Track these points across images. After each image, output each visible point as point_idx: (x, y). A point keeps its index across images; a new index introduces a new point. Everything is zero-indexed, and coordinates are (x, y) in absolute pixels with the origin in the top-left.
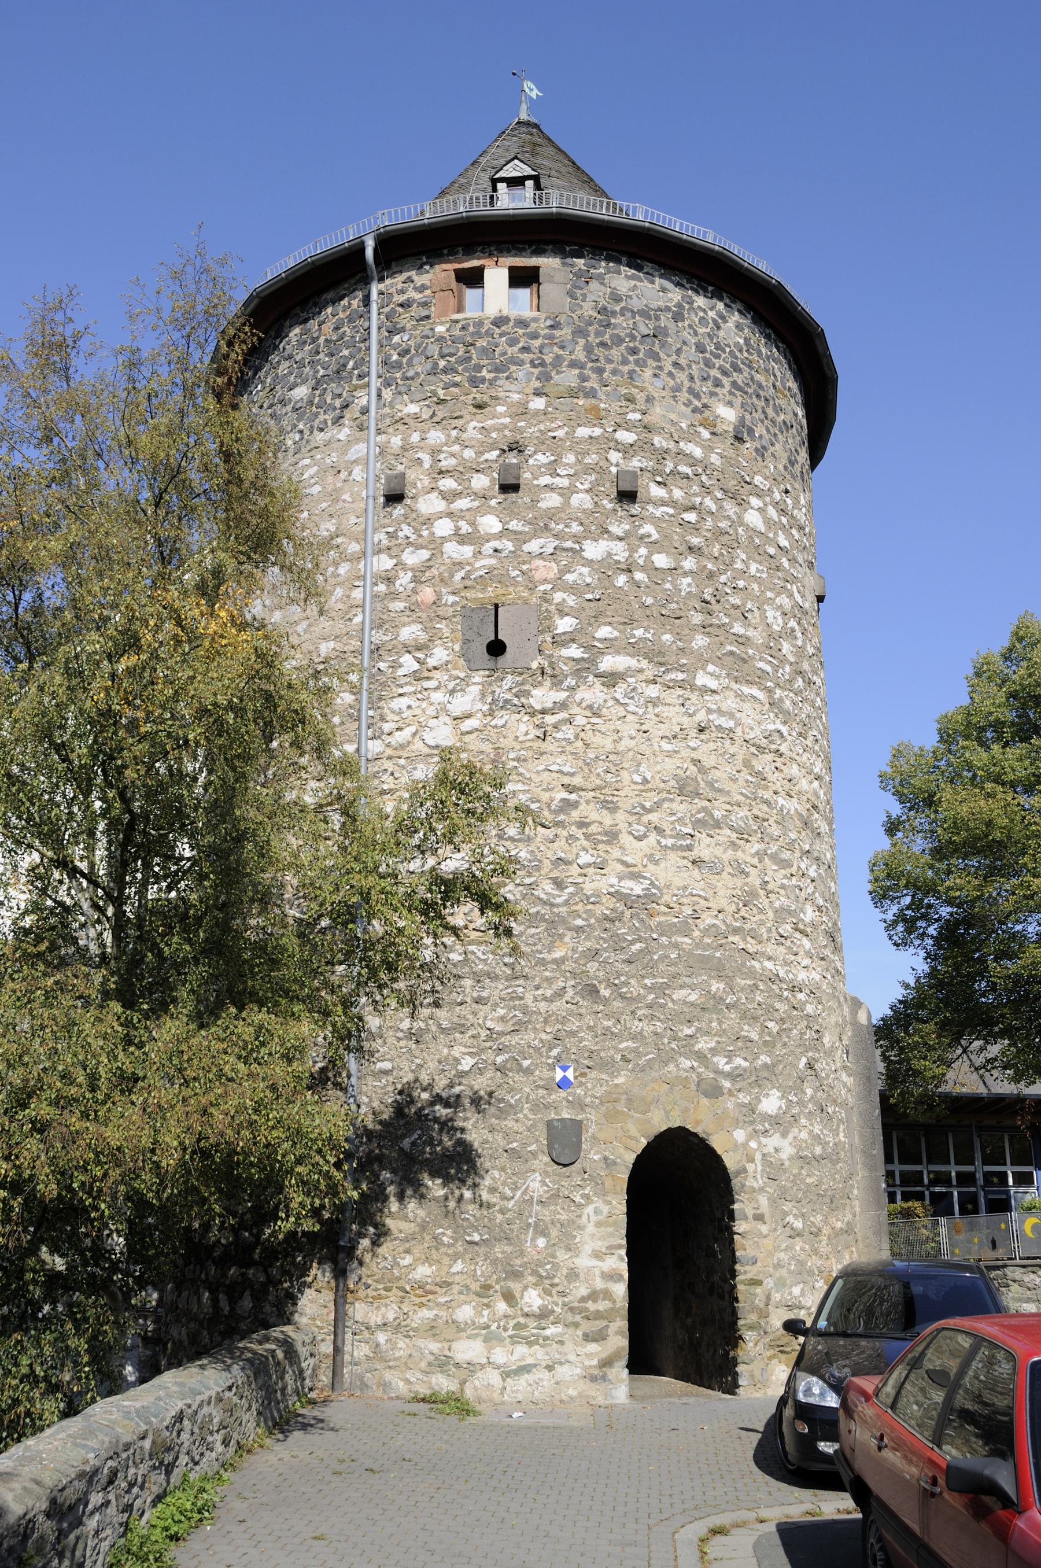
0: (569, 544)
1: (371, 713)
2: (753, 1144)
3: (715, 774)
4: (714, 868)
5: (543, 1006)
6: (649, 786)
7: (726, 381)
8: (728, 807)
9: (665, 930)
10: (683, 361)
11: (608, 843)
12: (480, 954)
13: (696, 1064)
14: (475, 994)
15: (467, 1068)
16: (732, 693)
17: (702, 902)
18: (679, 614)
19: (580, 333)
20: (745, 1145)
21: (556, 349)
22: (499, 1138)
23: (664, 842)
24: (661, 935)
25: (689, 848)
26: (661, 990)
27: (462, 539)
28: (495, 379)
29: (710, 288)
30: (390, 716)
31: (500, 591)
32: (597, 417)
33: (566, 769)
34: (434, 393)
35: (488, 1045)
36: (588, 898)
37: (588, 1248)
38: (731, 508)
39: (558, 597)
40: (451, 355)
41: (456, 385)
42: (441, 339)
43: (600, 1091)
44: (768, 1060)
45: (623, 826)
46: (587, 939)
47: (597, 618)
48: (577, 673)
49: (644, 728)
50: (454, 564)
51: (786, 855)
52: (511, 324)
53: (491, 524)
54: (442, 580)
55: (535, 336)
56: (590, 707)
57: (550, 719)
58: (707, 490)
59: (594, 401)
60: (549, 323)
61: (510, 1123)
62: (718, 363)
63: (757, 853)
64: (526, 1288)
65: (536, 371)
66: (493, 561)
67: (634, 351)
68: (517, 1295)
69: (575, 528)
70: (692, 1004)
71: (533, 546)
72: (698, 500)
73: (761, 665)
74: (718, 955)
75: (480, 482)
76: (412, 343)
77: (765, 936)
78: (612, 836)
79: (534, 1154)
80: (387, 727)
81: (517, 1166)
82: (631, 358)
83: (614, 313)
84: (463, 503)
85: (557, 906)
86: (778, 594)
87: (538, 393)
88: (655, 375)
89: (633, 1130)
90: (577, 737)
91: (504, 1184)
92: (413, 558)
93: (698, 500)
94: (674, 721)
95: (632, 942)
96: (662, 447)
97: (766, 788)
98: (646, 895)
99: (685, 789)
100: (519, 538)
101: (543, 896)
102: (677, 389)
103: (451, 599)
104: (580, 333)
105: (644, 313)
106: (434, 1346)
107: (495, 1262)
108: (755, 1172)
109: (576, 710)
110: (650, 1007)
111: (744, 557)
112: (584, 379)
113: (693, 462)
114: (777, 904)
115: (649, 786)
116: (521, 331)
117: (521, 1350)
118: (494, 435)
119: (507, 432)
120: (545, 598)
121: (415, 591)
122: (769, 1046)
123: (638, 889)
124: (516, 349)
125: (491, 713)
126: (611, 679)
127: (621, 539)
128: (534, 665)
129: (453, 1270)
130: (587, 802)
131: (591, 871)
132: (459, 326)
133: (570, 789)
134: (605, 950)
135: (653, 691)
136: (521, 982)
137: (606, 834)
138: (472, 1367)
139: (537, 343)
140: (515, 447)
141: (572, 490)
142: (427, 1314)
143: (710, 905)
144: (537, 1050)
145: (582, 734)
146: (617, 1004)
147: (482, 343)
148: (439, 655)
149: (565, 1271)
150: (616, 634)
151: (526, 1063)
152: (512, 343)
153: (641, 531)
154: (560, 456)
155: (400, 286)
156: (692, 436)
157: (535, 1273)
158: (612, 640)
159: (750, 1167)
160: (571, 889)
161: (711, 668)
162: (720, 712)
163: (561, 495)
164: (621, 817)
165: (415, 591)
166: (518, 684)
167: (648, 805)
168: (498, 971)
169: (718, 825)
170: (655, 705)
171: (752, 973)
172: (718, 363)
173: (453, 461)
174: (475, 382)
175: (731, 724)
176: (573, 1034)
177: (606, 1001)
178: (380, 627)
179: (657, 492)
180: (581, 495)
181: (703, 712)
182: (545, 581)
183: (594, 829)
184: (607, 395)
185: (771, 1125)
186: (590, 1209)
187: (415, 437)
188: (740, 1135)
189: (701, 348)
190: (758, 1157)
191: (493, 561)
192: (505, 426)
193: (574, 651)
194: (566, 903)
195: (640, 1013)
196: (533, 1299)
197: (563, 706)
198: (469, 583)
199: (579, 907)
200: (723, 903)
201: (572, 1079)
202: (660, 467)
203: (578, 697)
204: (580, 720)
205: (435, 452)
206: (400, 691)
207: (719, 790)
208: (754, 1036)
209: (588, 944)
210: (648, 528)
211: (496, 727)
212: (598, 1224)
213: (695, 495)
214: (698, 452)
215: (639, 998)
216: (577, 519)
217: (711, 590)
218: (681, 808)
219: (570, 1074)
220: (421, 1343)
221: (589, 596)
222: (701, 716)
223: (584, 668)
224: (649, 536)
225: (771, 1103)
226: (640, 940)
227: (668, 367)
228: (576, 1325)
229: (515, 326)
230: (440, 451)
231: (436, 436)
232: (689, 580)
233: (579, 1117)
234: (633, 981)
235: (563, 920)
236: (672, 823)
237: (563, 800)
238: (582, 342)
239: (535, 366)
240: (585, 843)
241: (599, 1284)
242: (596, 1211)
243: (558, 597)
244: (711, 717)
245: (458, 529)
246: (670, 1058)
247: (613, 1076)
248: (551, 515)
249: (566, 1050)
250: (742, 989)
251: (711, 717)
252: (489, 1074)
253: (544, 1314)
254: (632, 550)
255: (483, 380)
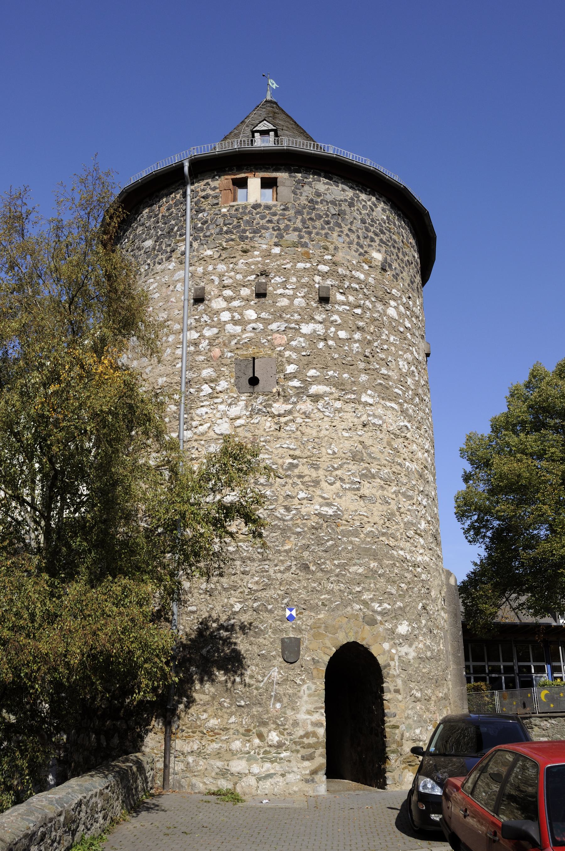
0: (293, 325)
1: (186, 416)
2: (394, 651)
3: (372, 449)
4: (372, 500)
5: (279, 575)
6: (336, 456)
7: (376, 239)
8: (379, 467)
9: (345, 534)
10: (354, 228)
11: (314, 486)
12: (244, 547)
13: (362, 607)
14: (242, 569)
15: (237, 610)
16: (381, 406)
17: (365, 519)
18: (352, 363)
19: (299, 212)
20: (389, 651)
21: (286, 221)
22: (255, 648)
23: (344, 486)
24: (343, 536)
25: (358, 489)
26: (343, 566)
27: (235, 323)
28: (254, 237)
29: (368, 190)
30: (196, 418)
31: (256, 351)
32: (308, 257)
33: (291, 447)
34: (221, 244)
35: (249, 597)
36: (303, 517)
37: (304, 709)
38: (380, 307)
39: (287, 353)
40: (230, 224)
41: (232, 240)
42: (224, 215)
43: (310, 622)
44: (402, 605)
45: (322, 477)
46: (303, 539)
47: (308, 365)
48: (297, 395)
49: (334, 424)
50: (231, 336)
51: (410, 493)
52: (262, 208)
53: (251, 314)
54: (224, 345)
55: (275, 214)
56: (304, 413)
57: (283, 420)
58: (367, 297)
59: (306, 249)
60: (282, 207)
61: (261, 640)
62: (372, 229)
63: (395, 492)
64: (270, 731)
65: (275, 233)
66: (252, 335)
67: (328, 223)
68: (265, 735)
69: (296, 317)
70: (360, 574)
71: (274, 326)
72: (362, 302)
73: (396, 390)
74: (374, 547)
75: (245, 292)
76: (209, 217)
77: (399, 537)
78: (316, 483)
79: (274, 657)
80: (194, 424)
81: (265, 663)
82: (326, 227)
83: (317, 203)
84: (236, 303)
85: (287, 521)
86: (405, 352)
87: (276, 245)
88: (339, 236)
89: (328, 644)
90: (297, 429)
91: (258, 673)
92: (208, 333)
93: (362, 302)
94: (350, 420)
95: (328, 541)
96: (343, 274)
97: (399, 457)
98: (335, 515)
99: (356, 457)
100: (267, 323)
101: (279, 516)
102: (351, 243)
103: (229, 354)
104: (299, 212)
105: (333, 203)
106: (219, 764)
107: (253, 717)
108: (395, 666)
109: (296, 415)
110: (337, 576)
111: (387, 332)
112: (301, 237)
113: (359, 281)
114: (406, 520)
115: (336, 456)
116: (267, 212)
117: (267, 765)
118: (253, 267)
119: (259, 266)
120: (280, 354)
121: (210, 350)
122: (402, 597)
123: (330, 512)
124: (264, 221)
125: (251, 416)
126: (316, 398)
127: (321, 323)
128: (274, 390)
129: (230, 721)
130: (303, 464)
131: (305, 502)
132: (234, 208)
133: (294, 457)
134: (313, 545)
135: (338, 404)
136: (267, 562)
137: (313, 482)
138: (240, 775)
139: (276, 218)
140: (264, 274)
141: (295, 296)
142: (215, 746)
143: (370, 520)
144: (276, 599)
145: (300, 428)
146: (320, 574)
147: (246, 218)
148: (223, 385)
149: (291, 722)
150: (318, 374)
151: (270, 607)
152: (263, 218)
153: (332, 319)
154: (288, 278)
155: (202, 187)
156: (359, 268)
157: (275, 722)
158: (316, 377)
159: (392, 663)
160: (294, 512)
161: (369, 392)
162: (374, 416)
163: (289, 299)
164: (321, 472)
165: (210, 350)
166: (265, 401)
167: (336, 466)
168: (254, 557)
169: (373, 476)
170: (339, 412)
171: (392, 557)
172: (372, 229)
173: (231, 281)
174: (242, 238)
175: (380, 422)
176: (295, 591)
177: (313, 573)
178: (191, 369)
179: (340, 297)
180: (299, 299)
181: (365, 416)
182: (280, 345)
183: (306, 479)
184: (313, 246)
185: (403, 640)
186: (305, 687)
187: (210, 268)
188: (386, 646)
189: (363, 221)
190: (396, 658)
191: (252, 335)
192: (259, 262)
193: (296, 383)
194: (292, 519)
195: (332, 579)
196: (274, 737)
197: (290, 412)
198: (239, 346)
199: (299, 521)
200: (377, 519)
201: (295, 615)
202: (342, 284)
203: (298, 407)
204: (299, 420)
205: (221, 276)
206: (202, 404)
207: (374, 458)
208: (394, 591)
209: (304, 542)
210: (335, 317)
211: (253, 423)
212: (310, 695)
213: (361, 299)
214: (362, 277)
215: (331, 571)
216: (297, 312)
217: (369, 350)
218: (354, 468)
219: (294, 613)
220: (212, 762)
221: (304, 353)
222: (364, 418)
223: (301, 392)
224: (336, 321)
225: (403, 628)
226: (332, 539)
227: (346, 231)
228: (298, 751)
229: (264, 209)
230: (224, 275)
231: (222, 267)
232: (357, 345)
233: (299, 637)
234: (328, 562)
235: (290, 529)
236: (349, 476)
237: (290, 463)
238: (300, 217)
239: (275, 230)
240: (302, 487)
241: (310, 728)
242: (308, 688)
243: (287, 353)
244: (370, 419)
245: (233, 317)
246: (346, 604)
247: (317, 614)
248: (284, 310)
249: (292, 600)
250: (387, 566)
251: (370, 419)
252: (250, 613)
253: (280, 745)
254: (327, 329)
255: (247, 238)
